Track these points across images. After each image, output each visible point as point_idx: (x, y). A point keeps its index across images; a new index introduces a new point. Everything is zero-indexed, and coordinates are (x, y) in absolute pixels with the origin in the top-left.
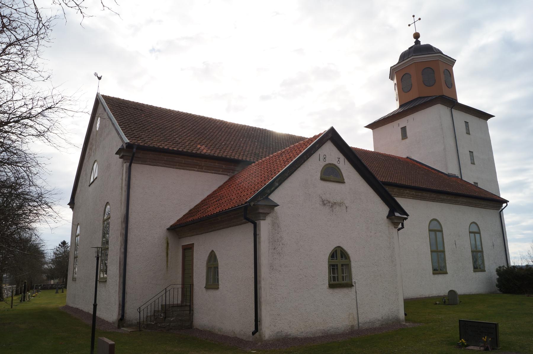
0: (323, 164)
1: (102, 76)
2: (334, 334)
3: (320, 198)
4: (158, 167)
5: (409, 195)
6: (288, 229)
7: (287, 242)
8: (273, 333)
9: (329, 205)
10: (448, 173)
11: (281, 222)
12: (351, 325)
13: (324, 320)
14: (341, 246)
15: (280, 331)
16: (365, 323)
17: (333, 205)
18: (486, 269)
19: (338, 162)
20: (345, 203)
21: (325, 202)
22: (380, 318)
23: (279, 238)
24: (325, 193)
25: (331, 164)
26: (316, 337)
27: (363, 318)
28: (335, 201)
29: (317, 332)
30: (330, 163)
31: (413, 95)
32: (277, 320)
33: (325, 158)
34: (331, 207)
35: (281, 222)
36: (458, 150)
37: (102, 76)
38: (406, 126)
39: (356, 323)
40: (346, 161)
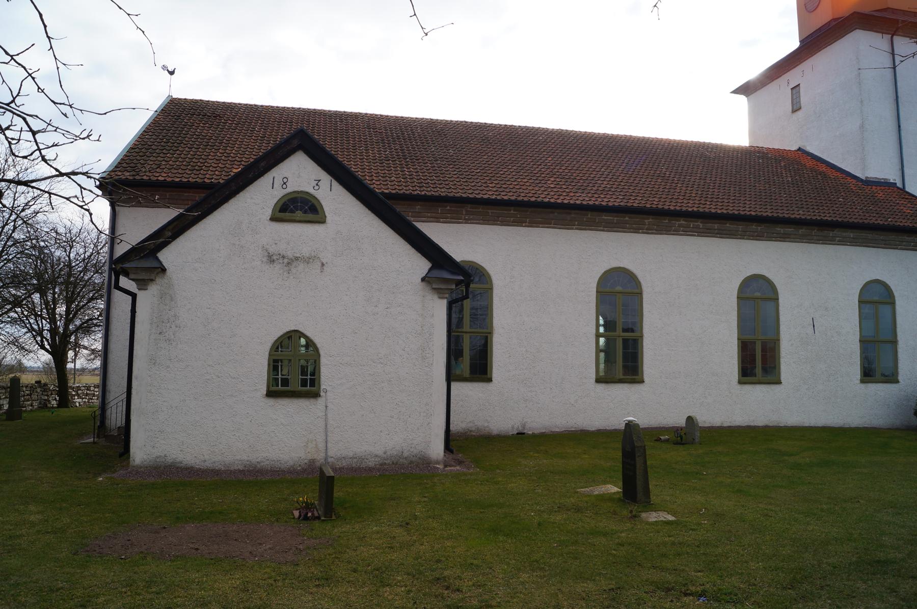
0: (278, 193)
1: (175, 69)
2: (269, 469)
3: (265, 251)
4: (159, 209)
5: (688, 229)
6: (189, 303)
7: (186, 323)
8: (149, 457)
9: (283, 263)
10: (867, 177)
11: (178, 292)
12: (311, 458)
13: (250, 446)
14: (300, 330)
15: (163, 455)
16: (344, 458)
17: (290, 262)
18: (900, 378)
19: (317, 188)
20: (320, 257)
21: (275, 257)
22: (380, 453)
23: (170, 316)
24: (276, 242)
25: (298, 192)
26: (231, 471)
27: (339, 450)
28: (298, 255)
29: (234, 463)
30: (296, 190)
31: (823, 16)
32: (158, 439)
33: (285, 183)
34: (286, 266)
35: (178, 292)
36: (899, 126)
37: (175, 69)
38: (799, 84)
39: (320, 457)
40: (335, 183)
